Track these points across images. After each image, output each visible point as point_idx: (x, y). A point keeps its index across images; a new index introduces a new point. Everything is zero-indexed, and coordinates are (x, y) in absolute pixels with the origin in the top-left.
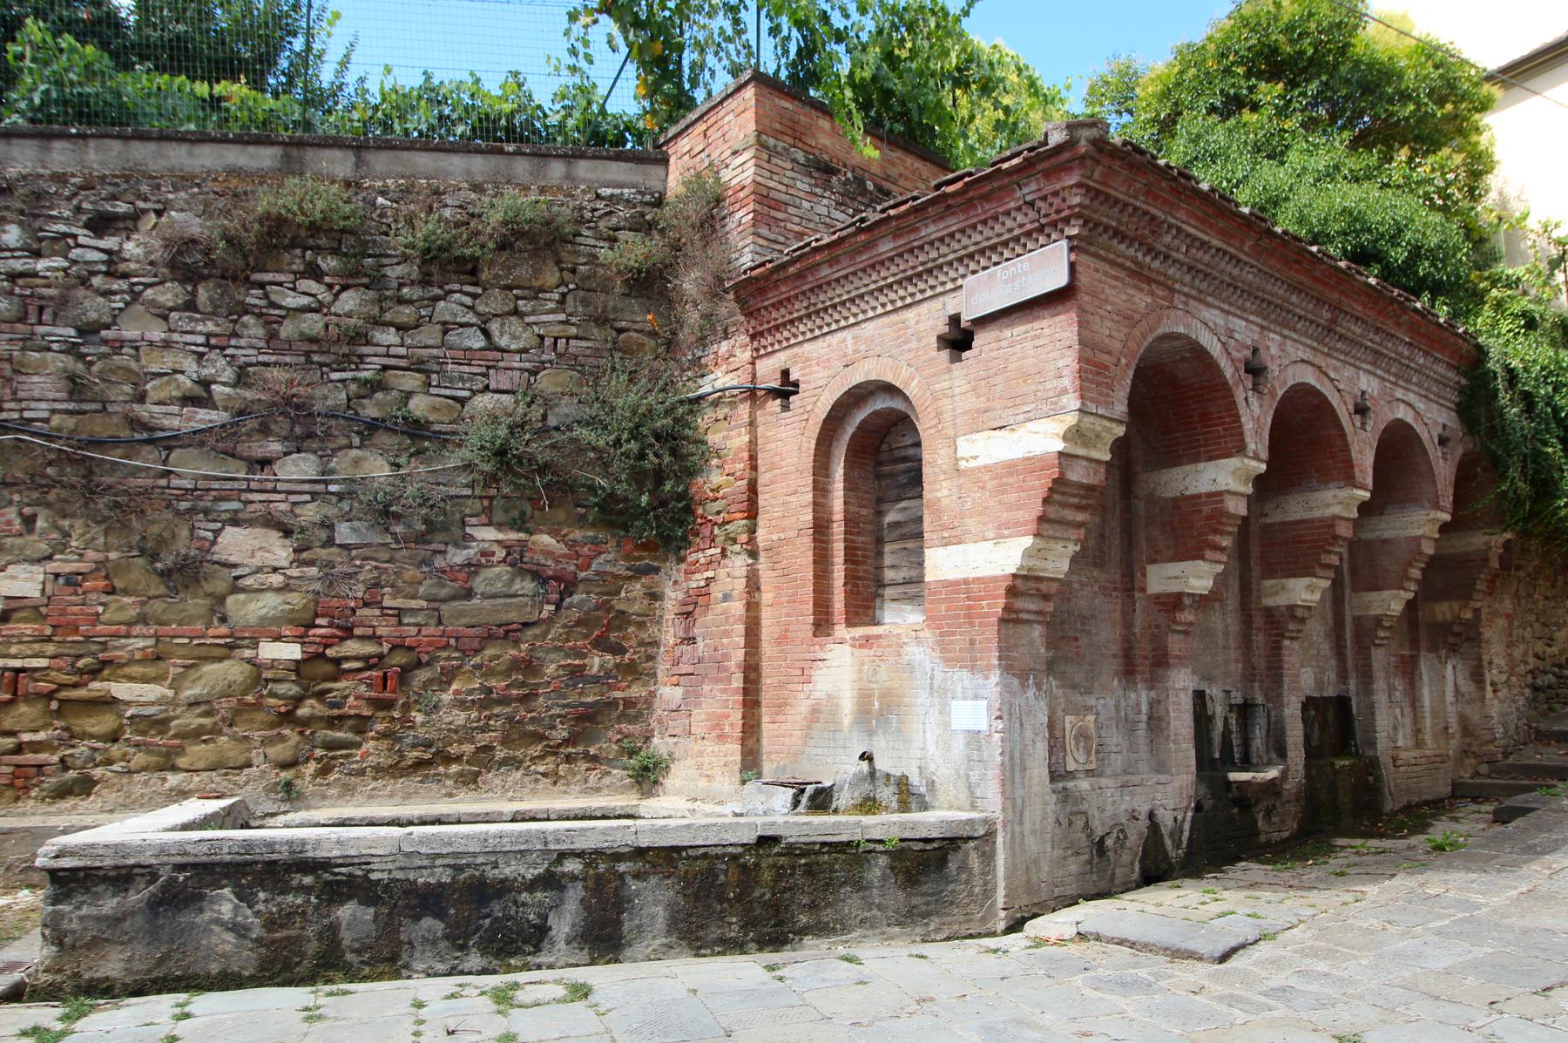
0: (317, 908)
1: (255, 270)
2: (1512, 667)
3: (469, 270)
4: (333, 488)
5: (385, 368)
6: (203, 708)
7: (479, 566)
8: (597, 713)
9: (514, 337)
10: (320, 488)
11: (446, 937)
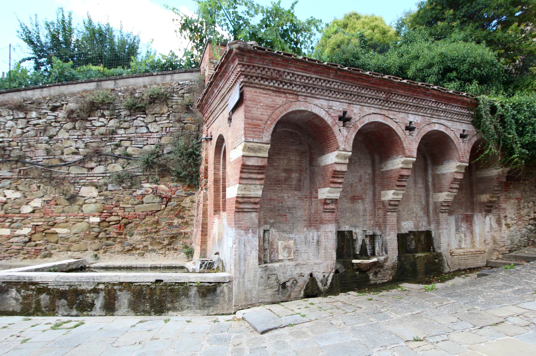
0: (36, 295)
1: (89, 116)
2: (520, 218)
3: (143, 110)
4: (108, 175)
5: (121, 140)
6: (77, 235)
7: (145, 195)
8: (177, 236)
9: (155, 128)
10: (104, 175)
11: (68, 305)
